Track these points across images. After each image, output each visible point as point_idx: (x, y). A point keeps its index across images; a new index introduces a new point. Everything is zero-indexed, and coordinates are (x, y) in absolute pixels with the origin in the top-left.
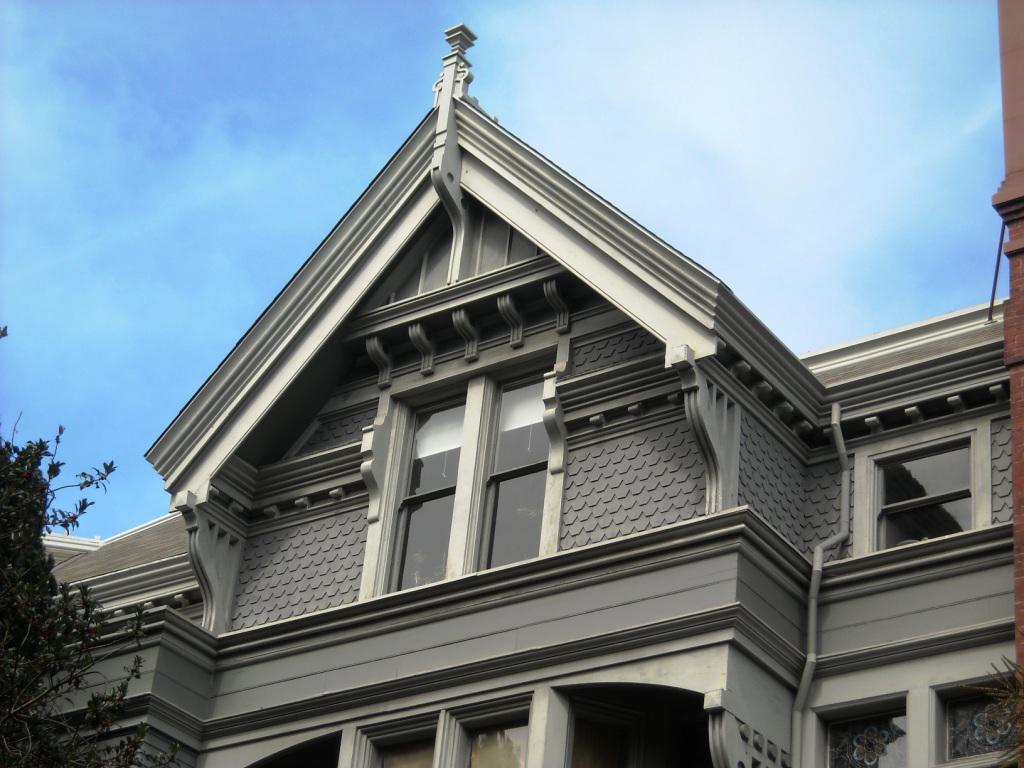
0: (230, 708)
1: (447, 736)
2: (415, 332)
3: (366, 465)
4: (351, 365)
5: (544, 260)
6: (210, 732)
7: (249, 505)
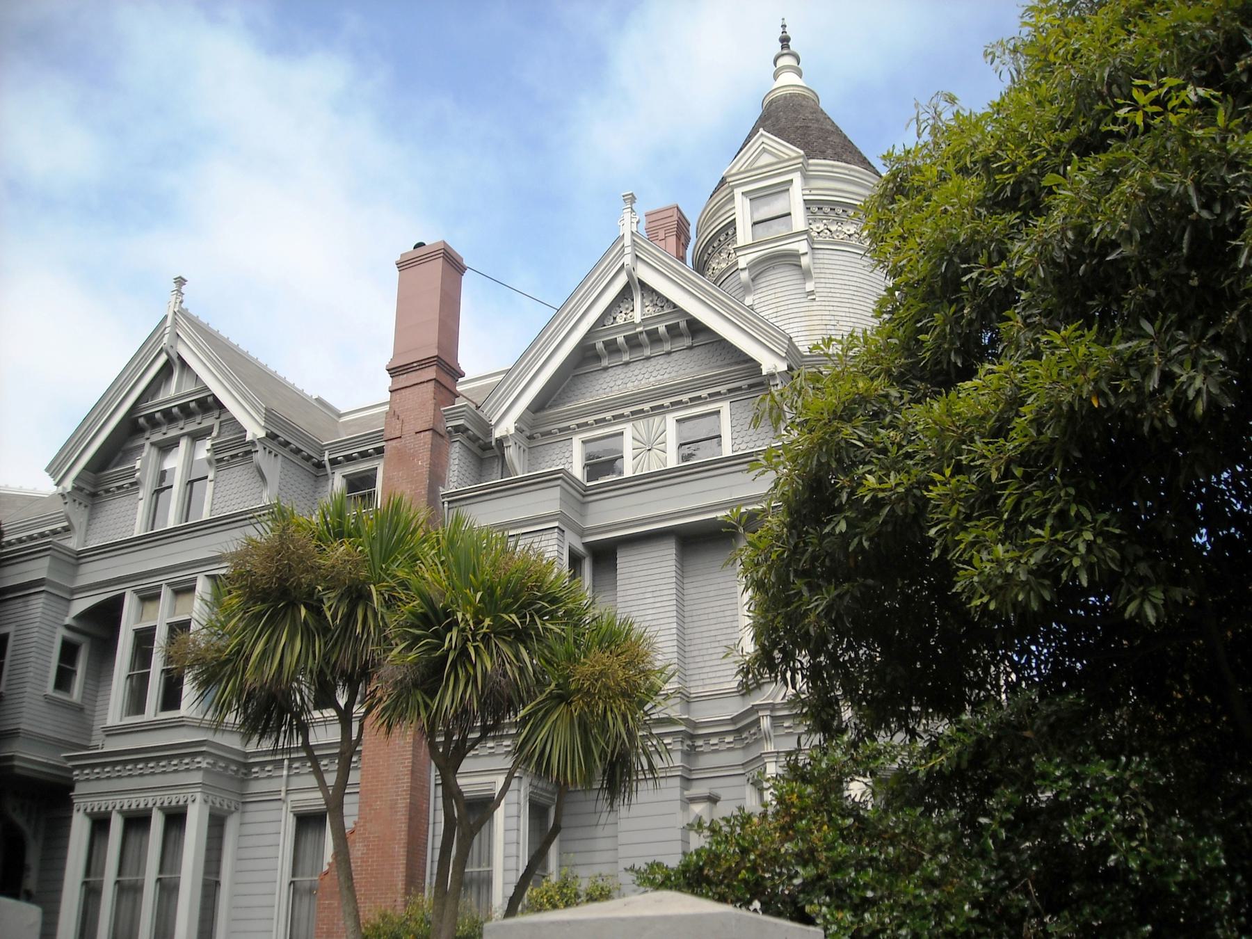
0: (82, 581)
1: (166, 593)
2: (175, 410)
3: (138, 474)
4: (132, 429)
5: (206, 388)
6: (73, 592)
7: (92, 490)
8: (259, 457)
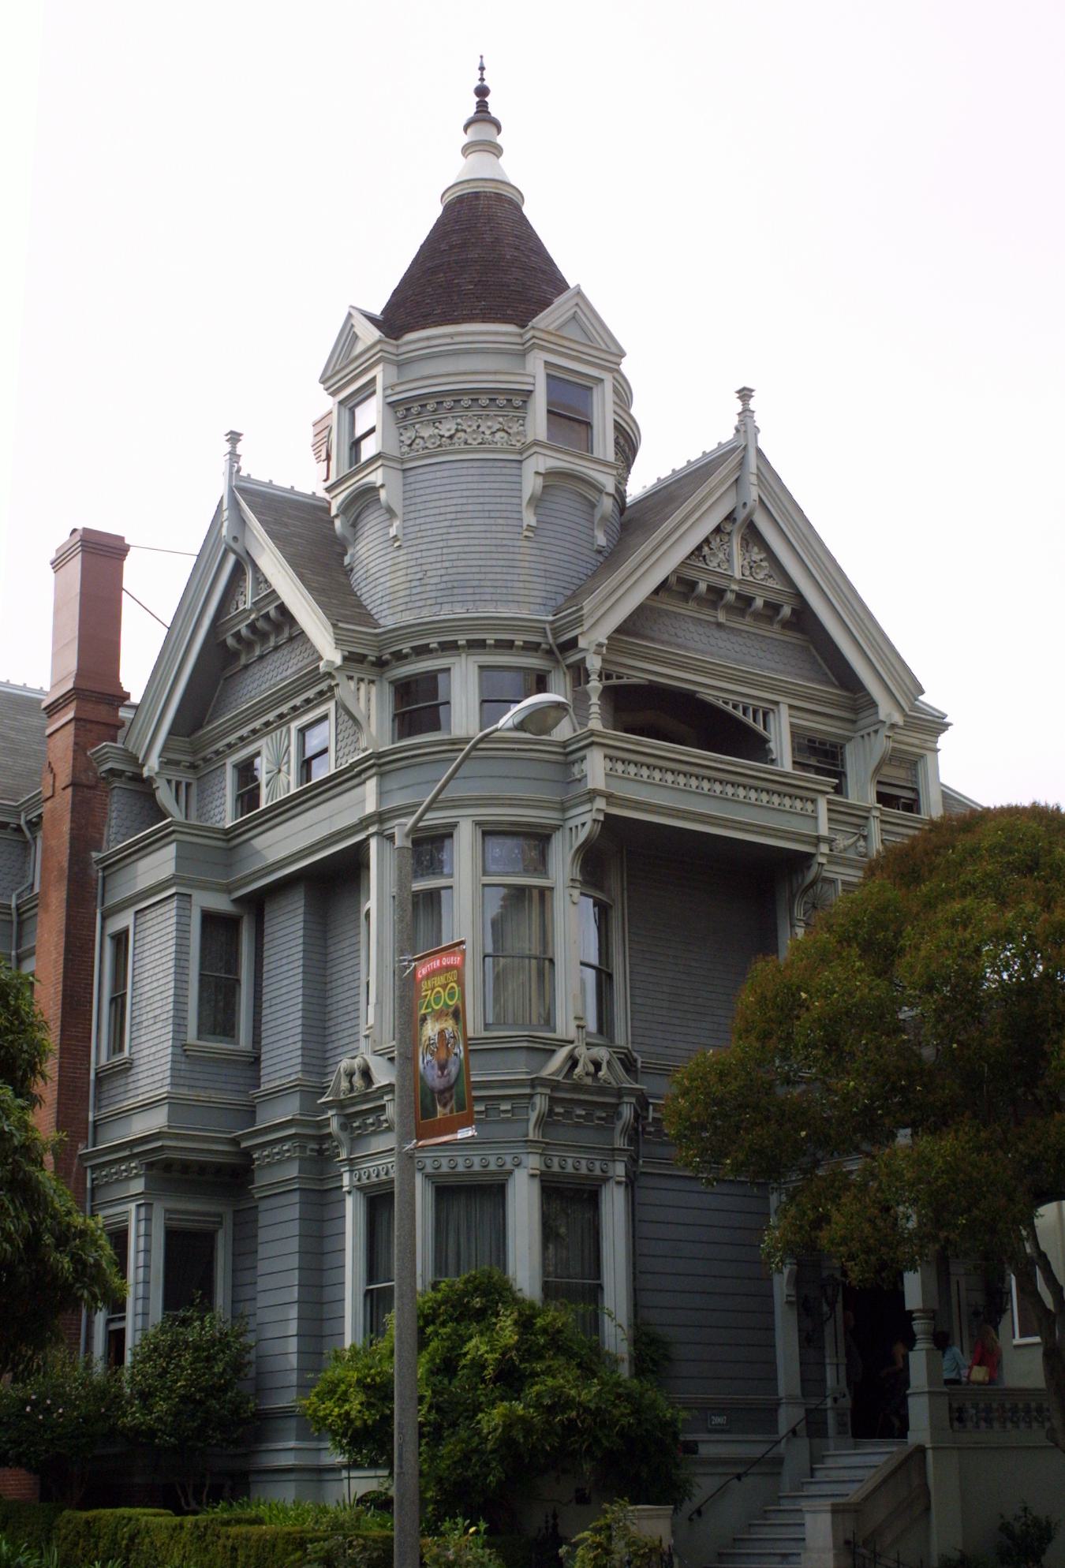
8: (346, 690)
